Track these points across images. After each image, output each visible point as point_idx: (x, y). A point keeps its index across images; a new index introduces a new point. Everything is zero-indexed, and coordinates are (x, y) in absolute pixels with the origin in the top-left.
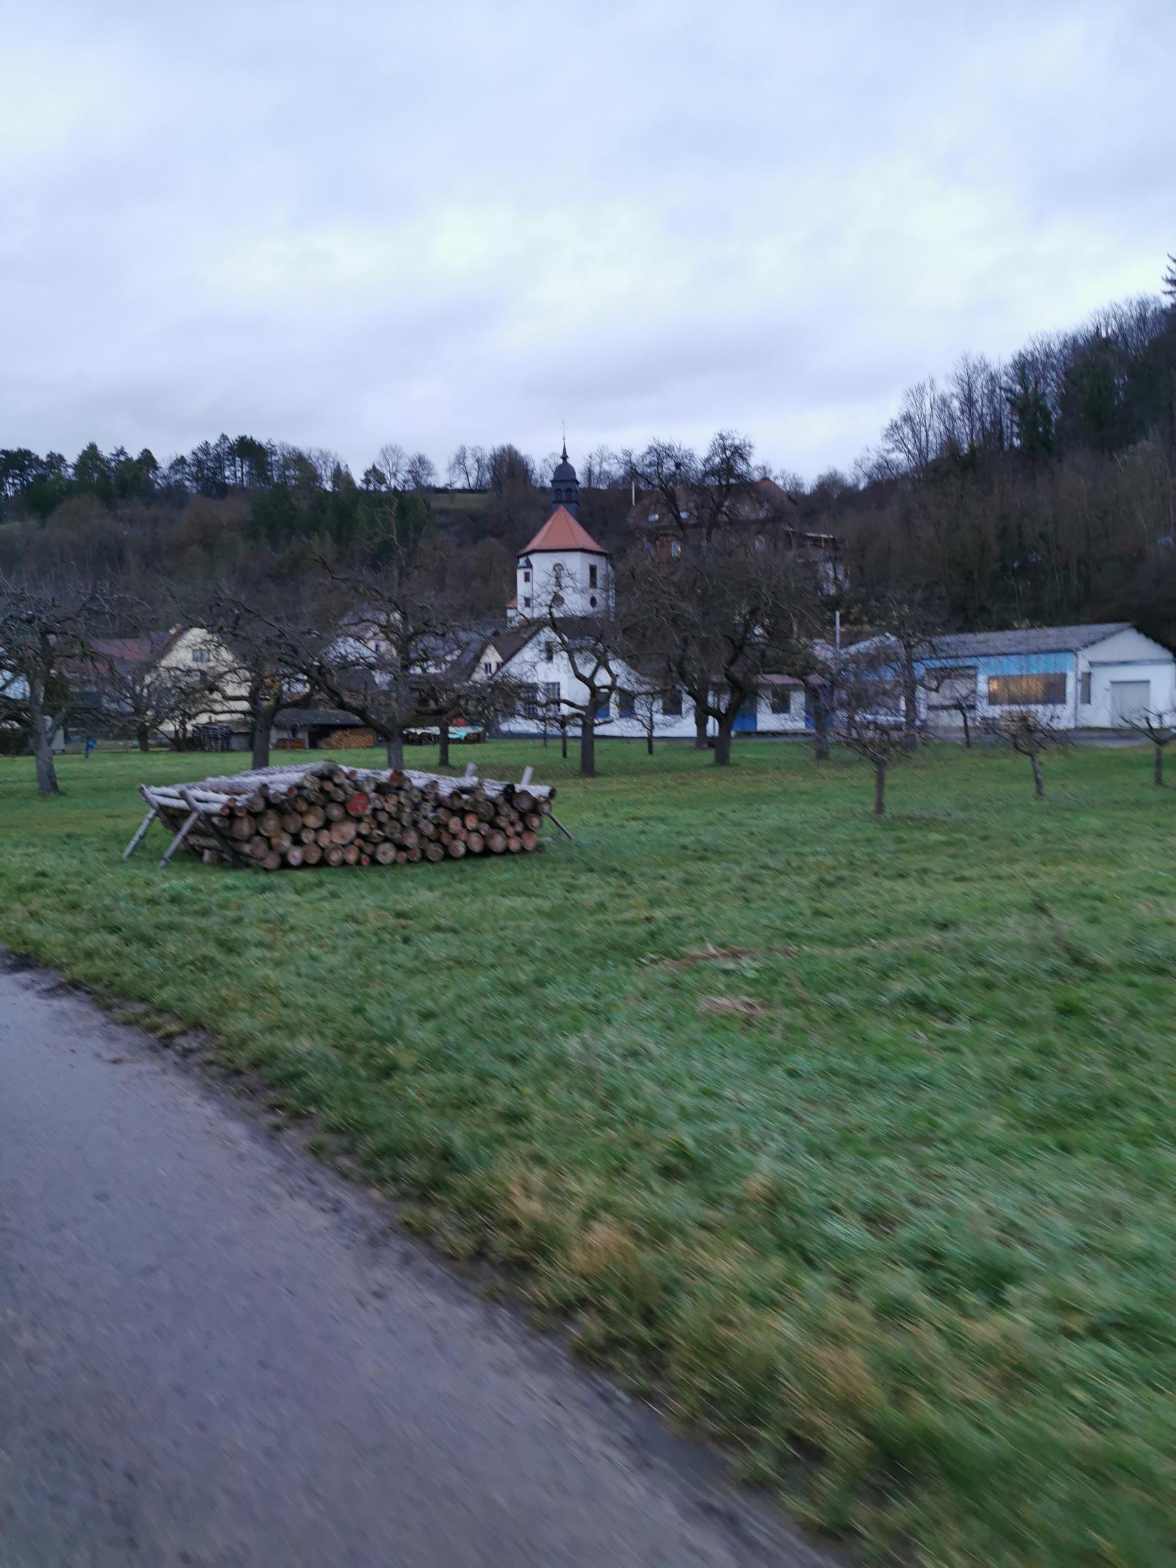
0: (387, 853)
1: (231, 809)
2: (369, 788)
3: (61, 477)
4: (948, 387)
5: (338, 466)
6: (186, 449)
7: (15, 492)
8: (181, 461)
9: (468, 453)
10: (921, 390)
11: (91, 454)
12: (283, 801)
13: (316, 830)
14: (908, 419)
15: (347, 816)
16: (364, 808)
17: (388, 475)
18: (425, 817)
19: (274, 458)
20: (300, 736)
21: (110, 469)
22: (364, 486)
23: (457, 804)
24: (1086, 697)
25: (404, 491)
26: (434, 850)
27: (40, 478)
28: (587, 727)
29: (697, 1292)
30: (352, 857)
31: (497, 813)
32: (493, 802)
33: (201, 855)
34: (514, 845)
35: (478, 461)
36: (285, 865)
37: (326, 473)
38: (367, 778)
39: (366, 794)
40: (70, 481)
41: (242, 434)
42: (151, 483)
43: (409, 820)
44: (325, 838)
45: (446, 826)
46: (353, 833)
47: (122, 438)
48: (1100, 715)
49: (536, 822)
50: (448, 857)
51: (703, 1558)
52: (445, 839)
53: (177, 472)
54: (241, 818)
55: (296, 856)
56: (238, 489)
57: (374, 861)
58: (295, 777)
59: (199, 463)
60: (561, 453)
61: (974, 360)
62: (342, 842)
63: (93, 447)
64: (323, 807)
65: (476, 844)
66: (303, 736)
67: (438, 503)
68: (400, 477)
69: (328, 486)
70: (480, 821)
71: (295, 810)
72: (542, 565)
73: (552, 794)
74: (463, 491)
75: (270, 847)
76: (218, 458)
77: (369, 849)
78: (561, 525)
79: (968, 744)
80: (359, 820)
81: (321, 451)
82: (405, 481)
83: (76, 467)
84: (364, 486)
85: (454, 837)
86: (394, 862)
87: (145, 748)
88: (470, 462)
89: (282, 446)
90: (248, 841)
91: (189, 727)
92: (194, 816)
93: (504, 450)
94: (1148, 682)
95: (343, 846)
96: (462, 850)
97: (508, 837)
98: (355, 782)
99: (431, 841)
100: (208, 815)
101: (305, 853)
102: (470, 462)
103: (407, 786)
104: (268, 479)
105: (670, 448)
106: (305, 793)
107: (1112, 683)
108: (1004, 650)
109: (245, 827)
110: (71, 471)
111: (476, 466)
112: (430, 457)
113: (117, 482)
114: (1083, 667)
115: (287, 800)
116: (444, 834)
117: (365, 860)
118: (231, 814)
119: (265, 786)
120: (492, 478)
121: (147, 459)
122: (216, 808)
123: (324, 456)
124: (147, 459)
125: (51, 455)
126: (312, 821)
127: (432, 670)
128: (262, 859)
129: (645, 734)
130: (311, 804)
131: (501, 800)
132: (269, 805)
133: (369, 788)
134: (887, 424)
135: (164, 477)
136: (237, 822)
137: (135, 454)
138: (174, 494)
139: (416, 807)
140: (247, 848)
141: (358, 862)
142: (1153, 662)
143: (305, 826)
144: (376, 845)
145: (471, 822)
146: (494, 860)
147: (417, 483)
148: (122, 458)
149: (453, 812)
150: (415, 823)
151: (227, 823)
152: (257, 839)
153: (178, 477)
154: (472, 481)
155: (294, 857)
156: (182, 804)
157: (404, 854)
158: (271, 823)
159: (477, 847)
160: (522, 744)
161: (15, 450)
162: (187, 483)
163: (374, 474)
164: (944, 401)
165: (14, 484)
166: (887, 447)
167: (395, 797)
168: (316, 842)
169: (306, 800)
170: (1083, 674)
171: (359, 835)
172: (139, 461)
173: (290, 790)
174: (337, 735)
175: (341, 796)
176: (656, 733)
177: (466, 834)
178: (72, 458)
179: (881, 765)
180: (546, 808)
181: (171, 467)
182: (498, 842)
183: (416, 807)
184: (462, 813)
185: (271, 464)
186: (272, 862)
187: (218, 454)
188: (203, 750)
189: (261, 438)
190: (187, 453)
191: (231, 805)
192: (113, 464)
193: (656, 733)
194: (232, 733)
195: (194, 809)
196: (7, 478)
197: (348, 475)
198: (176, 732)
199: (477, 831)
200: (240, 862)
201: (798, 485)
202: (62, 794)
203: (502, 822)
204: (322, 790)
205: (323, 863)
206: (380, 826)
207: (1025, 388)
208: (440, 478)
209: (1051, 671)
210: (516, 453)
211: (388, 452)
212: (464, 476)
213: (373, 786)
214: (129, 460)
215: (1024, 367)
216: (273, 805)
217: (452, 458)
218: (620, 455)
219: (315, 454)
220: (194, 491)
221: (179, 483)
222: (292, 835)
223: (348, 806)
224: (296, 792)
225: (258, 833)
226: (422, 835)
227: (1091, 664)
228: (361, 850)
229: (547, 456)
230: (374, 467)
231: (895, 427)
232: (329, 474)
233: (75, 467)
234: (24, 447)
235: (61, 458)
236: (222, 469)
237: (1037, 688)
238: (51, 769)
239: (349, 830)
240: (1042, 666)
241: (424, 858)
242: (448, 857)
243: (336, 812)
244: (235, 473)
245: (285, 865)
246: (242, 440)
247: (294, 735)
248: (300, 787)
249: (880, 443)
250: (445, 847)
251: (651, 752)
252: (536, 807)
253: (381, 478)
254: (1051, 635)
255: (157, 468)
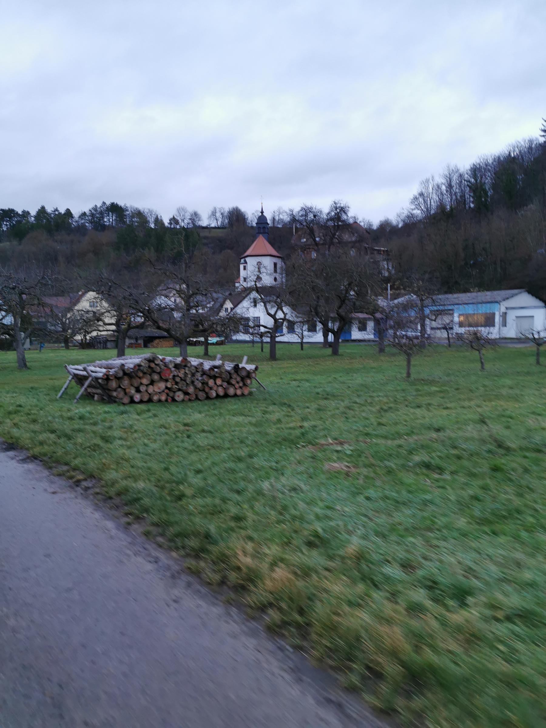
0: (180, 396)
1: (107, 375)
2: (171, 366)
3: (28, 222)
4: (440, 180)
5: (157, 216)
6: (86, 208)
7: (7, 228)
8: (84, 214)
9: (217, 210)
10: (427, 181)
11: (42, 211)
12: (131, 372)
13: (147, 385)
14: (421, 194)
15: (161, 379)
16: (169, 375)
17: (180, 221)
18: (197, 380)
19: (127, 213)
20: (139, 342)
21: (51, 218)
22: (169, 226)
23: (212, 373)
24: (504, 324)
25: (187, 228)
26: (201, 395)
27: (19, 222)
28: (273, 338)
29: (324, 600)
30: (163, 398)
31: (231, 378)
32: (229, 372)
33: (93, 397)
34: (239, 392)
35: (222, 214)
36: (132, 401)
37: (151, 220)
38: (171, 361)
39: (170, 369)
40: (33, 223)
41: (112, 202)
42: (70, 224)
43: (190, 380)
44: (151, 389)
45: (207, 384)
46: (164, 387)
47: (57, 204)
48: (510, 332)
49: (249, 381)
50: (208, 398)
51: (326, 724)
52: (207, 390)
53: (82, 219)
54: (112, 380)
55: (137, 397)
56: (111, 227)
57: (174, 400)
58: (137, 361)
59: (92, 215)
60: (260, 210)
61: (452, 167)
62: (159, 391)
63: (43, 208)
64: (150, 375)
65: (221, 392)
66: (141, 342)
67: (203, 234)
68: (186, 221)
69: (152, 226)
70: (223, 381)
71: (137, 376)
72: (252, 262)
73: (256, 369)
74: (215, 228)
75: (126, 393)
76: (101, 213)
77: (171, 394)
78: (261, 244)
79: (450, 346)
80: (167, 381)
81: (149, 209)
82: (188, 224)
83: (35, 217)
84: (169, 226)
85: (211, 388)
86: (183, 400)
87: (67, 347)
88: (218, 215)
89: (131, 207)
90: (115, 390)
91: (88, 338)
92: (90, 379)
93: (234, 209)
94: (533, 317)
95: (159, 393)
96: (214, 394)
97: (236, 388)
98: (165, 363)
99: (200, 390)
100: (97, 379)
101: (141, 396)
102: (218, 215)
103: (189, 365)
104: (125, 223)
105: (311, 208)
106: (142, 368)
107: (516, 317)
108: (466, 302)
109: (114, 384)
110: (33, 219)
111: (221, 217)
112: (199, 212)
113: (54, 224)
114: (503, 309)
115: (133, 372)
116: (206, 387)
117: (170, 399)
118: (107, 378)
119: (123, 365)
120: (229, 222)
121: (68, 213)
122: (100, 375)
123: (151, 212)
124: (68, 213)
125: (24, 211)
126: (145, 381)
127: (201, 311)
128: (122, 399)
129: (299, 341)
130: (145, 373)
131: (233, 371)
132: (125, 374)
133: (171, 366)
134: (412, 197)
135: (76, 222)
136: (110, 382)
137: (62, 211)
138: (81, 230)
139: (193, 375)
140: (115, 394)
141: (166, 400)
142: (535, 307)
143: (141, 384)
144: (174, 392)
145: (219, 382)
146: (229, 399)
147: (194, 224)
148: (57, 213)
149: (210, 377)
150: (193, 382)
151: (106, 382)
152: (119, 389)
153: (83, 221)
154: (219, 223)
155: (137, 398)
156: (84, 373)
157: (188, 397)
158: (126, 382)
159: (221, 393)
160: (242, 345)
161: (7, 209)
162: (87, 224)
163: (174, 220)
164: (438, 186)
165: (6, 225)
166: (412, 208)
167: (183, 370)
168: (147, 391)
169: (142, 371)
170: (503, 313)
171: (167, 388)
172: (65, 214)
173: (135, 367)
174: (157, 341)
175: (158, 370)
176: (305, 341)
177: (217, 387)
178: (33, 213)
179: (409, 355)
180: (253, 375)
181: (80, 217)
182: (231, 391)
183: (193, 375)
184: (214, 378)
185: (126, 215)
186: (126, 400)
187: (101, 211)
188: (94, 348)
189: (121, 203)
190: (87, 210)
191: (107, 374)
192: (52, 215)
193: (305, 341)
194: (108, 340)
195: (90, 376)
196: (3, 222)
197: (162, 220)
198: (82, 340)
199: (221, 386)
200: (112, 400)
201: (371, 225)
202: (29, 369)
203: (233, 382)
204: (149, 367)
205: (150, 401)
206: (177, 383)
207: (476, 180)
208: (204, 222)
209: (488, 312)
210: (240, 210)
211: (180, 210)
212: (215, 221)
213: (173, 365)
214: (60, 213)
215: (476, 170)
216: (127, 374)
217: (210, 213)
218: (288, 211)
219: (146, 211)
220: (90, 228)
221: (83, 224)
222: (136, 388)
223: (161, 374)
224: (137, 368)
225: (120, 387)
226: (196, 388)
227: (507, 308)
228: (168, 395)
229: (254, 212)
230: (174, 217)
231: (416, 198)
232: (153, 220)
233: (35, 217)
234: (11, 207)
235: (28, 213)
236: (103, 218)
237: (482, 320)
238: (24, 357)
239: (162, 385)
240: (484, 309)
241: (197, 398)
242: (208, 398)
243: (156, 377)
244: (109, 220)
245: (132, 401)
246: (113, 204)
247: (137, 341)
248: (139, 365)
249: (409, 206)
250: (207, 393)
251: (302, 349)
252: (249, 375)
253: (177, 222)
254: (488, 295)
255: (73, 217)
